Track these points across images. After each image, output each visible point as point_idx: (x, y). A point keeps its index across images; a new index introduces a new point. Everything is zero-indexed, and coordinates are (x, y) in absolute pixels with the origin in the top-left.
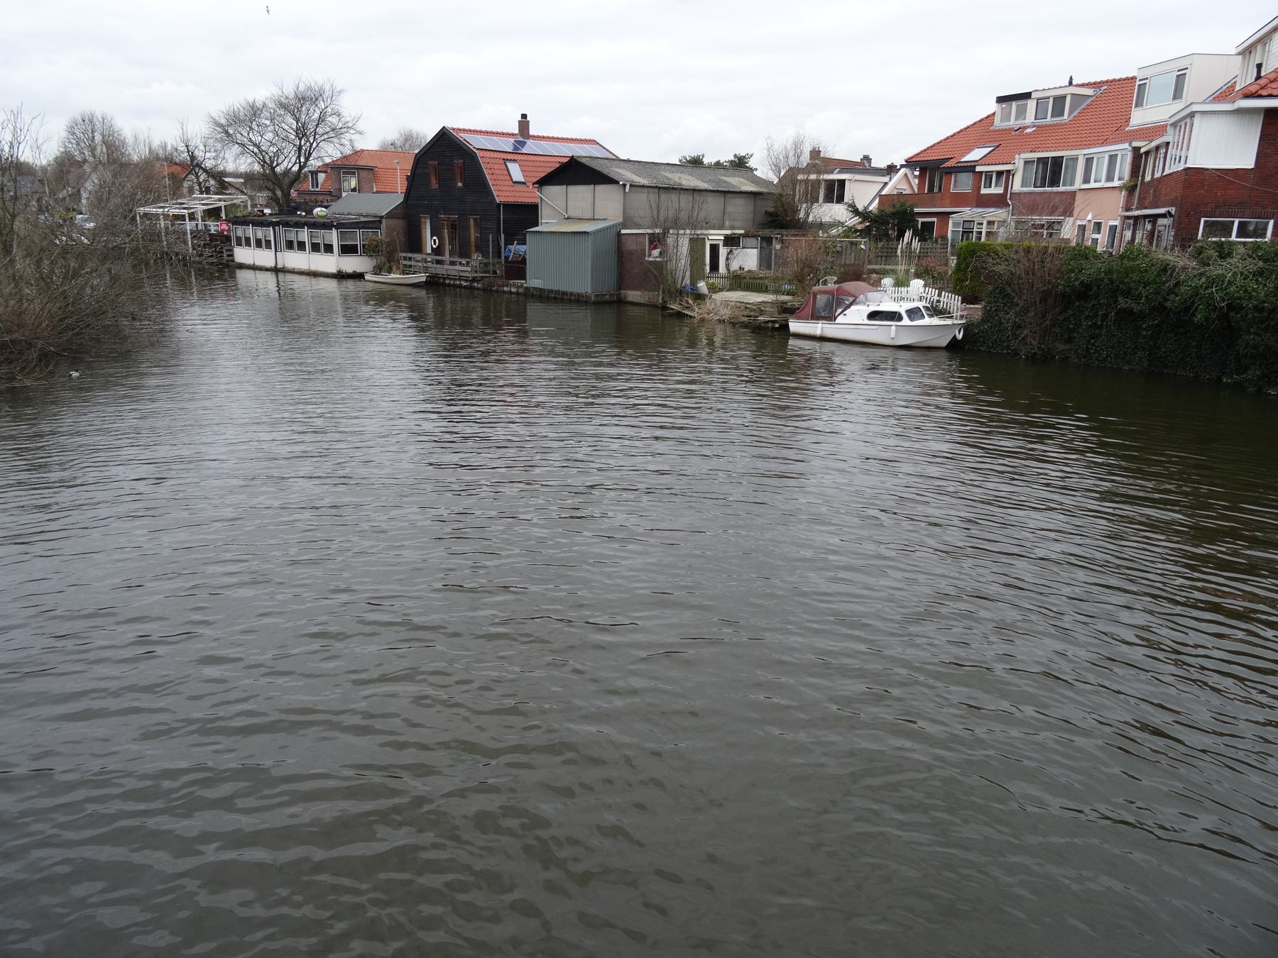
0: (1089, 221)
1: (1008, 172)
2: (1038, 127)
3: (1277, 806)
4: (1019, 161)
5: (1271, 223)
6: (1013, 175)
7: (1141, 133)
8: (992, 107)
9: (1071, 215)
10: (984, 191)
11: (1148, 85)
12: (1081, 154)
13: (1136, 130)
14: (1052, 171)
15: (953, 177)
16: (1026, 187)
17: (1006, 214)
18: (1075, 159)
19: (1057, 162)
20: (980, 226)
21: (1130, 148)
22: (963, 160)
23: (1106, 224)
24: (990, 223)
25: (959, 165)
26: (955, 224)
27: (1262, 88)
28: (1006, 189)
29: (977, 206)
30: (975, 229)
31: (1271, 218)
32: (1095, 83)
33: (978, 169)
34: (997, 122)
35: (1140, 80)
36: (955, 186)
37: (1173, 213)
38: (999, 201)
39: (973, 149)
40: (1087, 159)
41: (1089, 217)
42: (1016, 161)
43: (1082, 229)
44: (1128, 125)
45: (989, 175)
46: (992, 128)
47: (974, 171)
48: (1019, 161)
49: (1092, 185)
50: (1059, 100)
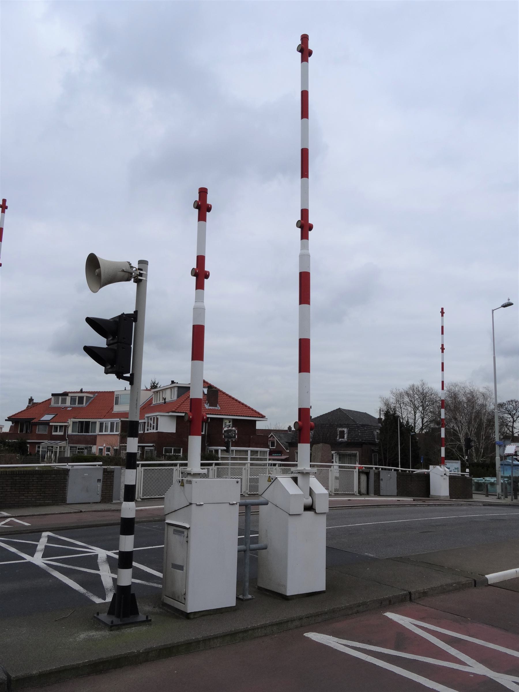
0: (104, 447)
1: (66, 426)
2: (73, 408)
4: (70, 422)
5: (182, 449)
7: (115, 415)
8: (50, 396)
9: (95, 444)
10: (54, 433)
11: (119, 397)
12: (98, 421)
13: (116, 413)
14: (85, 427)
16: (74, 432)
18: (95, 423)
19: (88, 423)
20: (56, 449)
21: (120, 421)
22: (41, 420)
24: (60, 447)
25: (39, 422)
26: (43, 448)
27: (176, 410)
28: (65, 433)
29: (51, 440)
30: (54, 450)
31: (182, 448)
33: (51, 424)
34: (53, 404)
35: (116, 395)
36: (38, 431)
37: (155, 445)
38: (62, 438)
39: (45, 415)
40: (100, 423)
42: (69, 422)
43: (101, 450)
44: (113, 411)
45: (56, 427)
46: (113, 412)
47: (49, 425)
48: (70, 422)
49: (104, 433)
50: (81, 399)
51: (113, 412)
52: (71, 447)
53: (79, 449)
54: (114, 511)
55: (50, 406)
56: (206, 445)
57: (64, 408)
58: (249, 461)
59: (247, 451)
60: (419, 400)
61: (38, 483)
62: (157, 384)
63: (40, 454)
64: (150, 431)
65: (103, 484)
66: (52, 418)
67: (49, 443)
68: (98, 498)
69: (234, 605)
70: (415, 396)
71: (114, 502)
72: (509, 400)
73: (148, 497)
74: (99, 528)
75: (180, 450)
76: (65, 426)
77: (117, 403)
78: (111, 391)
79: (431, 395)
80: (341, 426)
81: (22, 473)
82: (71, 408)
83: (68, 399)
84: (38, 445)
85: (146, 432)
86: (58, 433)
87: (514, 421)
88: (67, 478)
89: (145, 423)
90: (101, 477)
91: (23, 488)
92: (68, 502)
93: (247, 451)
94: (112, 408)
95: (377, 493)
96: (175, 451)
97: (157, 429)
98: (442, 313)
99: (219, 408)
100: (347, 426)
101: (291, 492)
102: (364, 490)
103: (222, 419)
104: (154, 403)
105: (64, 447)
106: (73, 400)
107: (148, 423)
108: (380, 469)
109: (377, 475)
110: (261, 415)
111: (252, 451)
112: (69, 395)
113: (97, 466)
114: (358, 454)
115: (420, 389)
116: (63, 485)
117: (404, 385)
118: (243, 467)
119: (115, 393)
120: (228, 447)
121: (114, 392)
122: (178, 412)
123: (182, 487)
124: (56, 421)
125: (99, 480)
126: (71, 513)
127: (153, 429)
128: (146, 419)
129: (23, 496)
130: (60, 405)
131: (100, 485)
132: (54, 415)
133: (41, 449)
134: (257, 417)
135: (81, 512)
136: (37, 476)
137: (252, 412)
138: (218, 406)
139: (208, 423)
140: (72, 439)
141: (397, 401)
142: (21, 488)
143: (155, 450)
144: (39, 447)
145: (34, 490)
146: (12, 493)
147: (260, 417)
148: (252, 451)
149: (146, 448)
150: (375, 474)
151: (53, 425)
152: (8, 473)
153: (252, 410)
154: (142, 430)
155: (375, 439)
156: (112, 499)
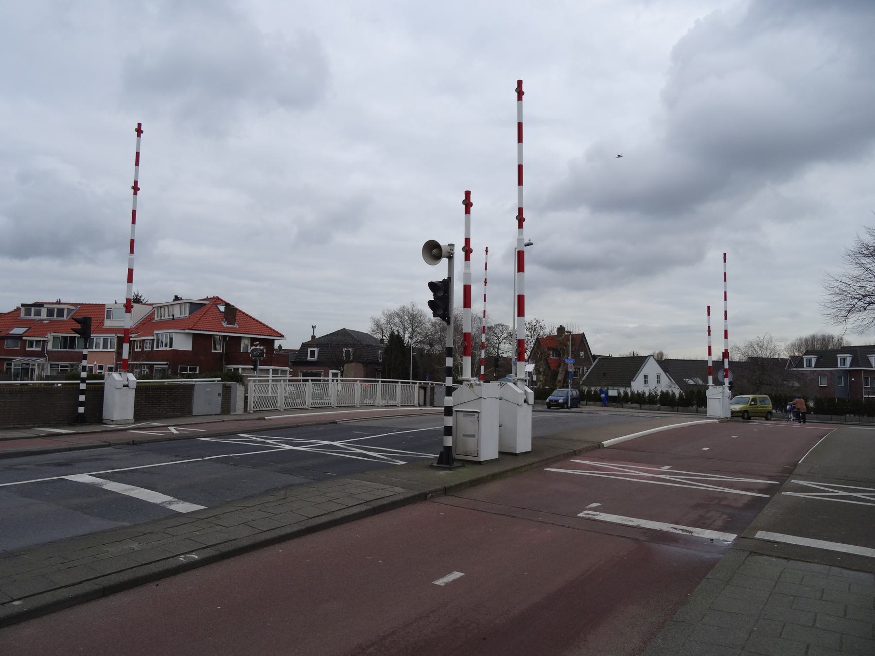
1: (44, 341)
2: (50, 320)
3: (1, 605)
6: (47, 343)
8: (20, 306)
10: (28, 349)
13: (108, 328)
15: (6, 341)
17: (44, 361)
22: (10, 333)
23: (106, 366)
25: (8, 335)
26: (15, 365)
30: (30, 368)
32: (75, 304)
33: (24, 338)
34: (22, 315)
38: (40, 355)
39: (14, 328)
41: (95, 363)
46: (103, 327)
47: (22, 339)
48: (50, 336)
51: (103, 327)
52: (51, 365)
53: (62, 367)
54: (249, 420)
55: (19, 318)
56: (224, 363)
57: (39, 320)
58: (271, 378)
59: (269, 370)
60: (409, 321)
61: (169, 397)
62: (140, 297)
63: (11, 372)
64: (160, 349)
65: (222, 397)
66: (25, 332)
67: (22, 359)
68: (219, 411)
69: (498, 457)
70: (405, 317)
71: (232, 413)
72: (497, 324)
73: (258, 409)
74: (174, 441)
75: (196, 368)
76: (43, 341)
77: (109, 317)
78: (101, 303)
79: (421, 316)
80: (347, 346)
81: (155, 387)
82: (48, 321)
83: (44, 312)
84: (9, 362)
85: (155, 349)
86: (34, 349)
87: (500, 343)
88: (193, 392)
89: (153, 340)
90: (221, 392)
91: (156, 401)
92: (193, 415)
93: (269, 370)
94: (102, 323)
95: (432, 405)
96: (191, 370)
97: (171, 346)
98: (487, 251)
99: (238, 327)
100: (353, 346)
101: (519, 392)
102: (422, 403)
103: (240, 338)
104: (156, 319)
105: (43, 365)
106: (50, 313)
107: (158, 340)
108: (434, 385)
109: (433, 389)
110: (280, 334)
111: (273, 370)
112: (45, 306)
113: (216, 382)
114: (323, 372)
115: (410, 311)
116: (189, 399)
117: (395, 307)
118: (279, 383)
119: (107, 307)
120: (255, 366)
121: (105, 305)
122: (195, 330)
123: (471, 388)
124: (36, 336)
125: (219, 394)
126: (216, 422)
127: (166, 346)
128: (155, 336)
129: (156, 409)
130: (32, 316)
131: (220, 398)
132: (27, 329)
133: (13, 367)
134: (276, 336)
135: (224, 421)
136: (168, 391)
137: (270, 331)
138: (236, 324)
139: (227, 341)
140: (52, 356)
141: (388, 322)
142: (154, 401)
143: (169, 368)
144: (11, 364)
145: (165, 403)
146: (146, 406)
147: (279, 336)
148: (273, 370)
149: (155, 366)
150: (431, 388)
151: (26, 340)
152: (23, 390)
153: (271, 329)
154: (140, 346)
155: (378, 358)
156: (230, 411)
